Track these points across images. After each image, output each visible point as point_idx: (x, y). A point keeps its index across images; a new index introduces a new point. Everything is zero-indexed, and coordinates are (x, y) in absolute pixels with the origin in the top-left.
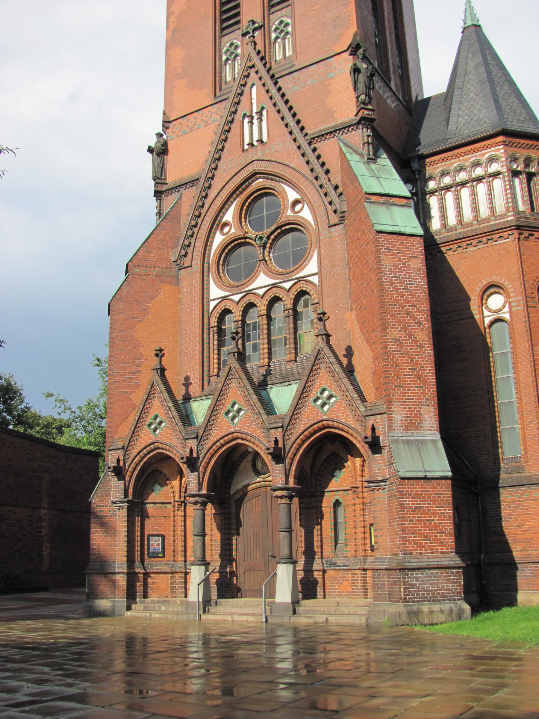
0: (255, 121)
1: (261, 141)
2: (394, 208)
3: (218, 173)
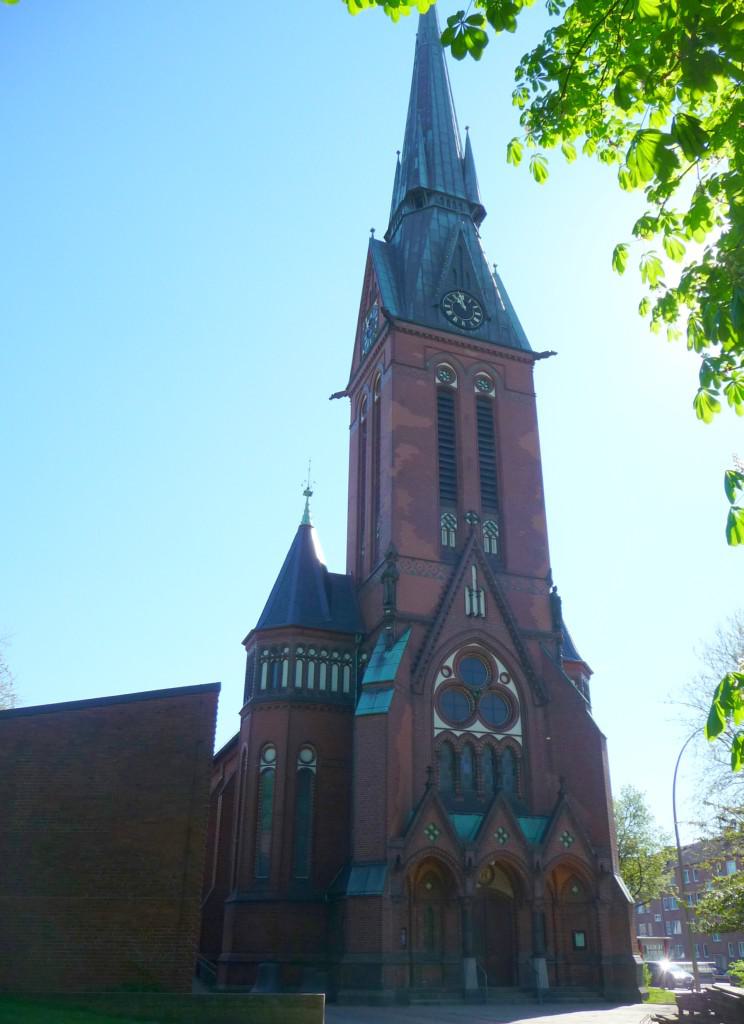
0: (475, 594)
1: (479, 614)
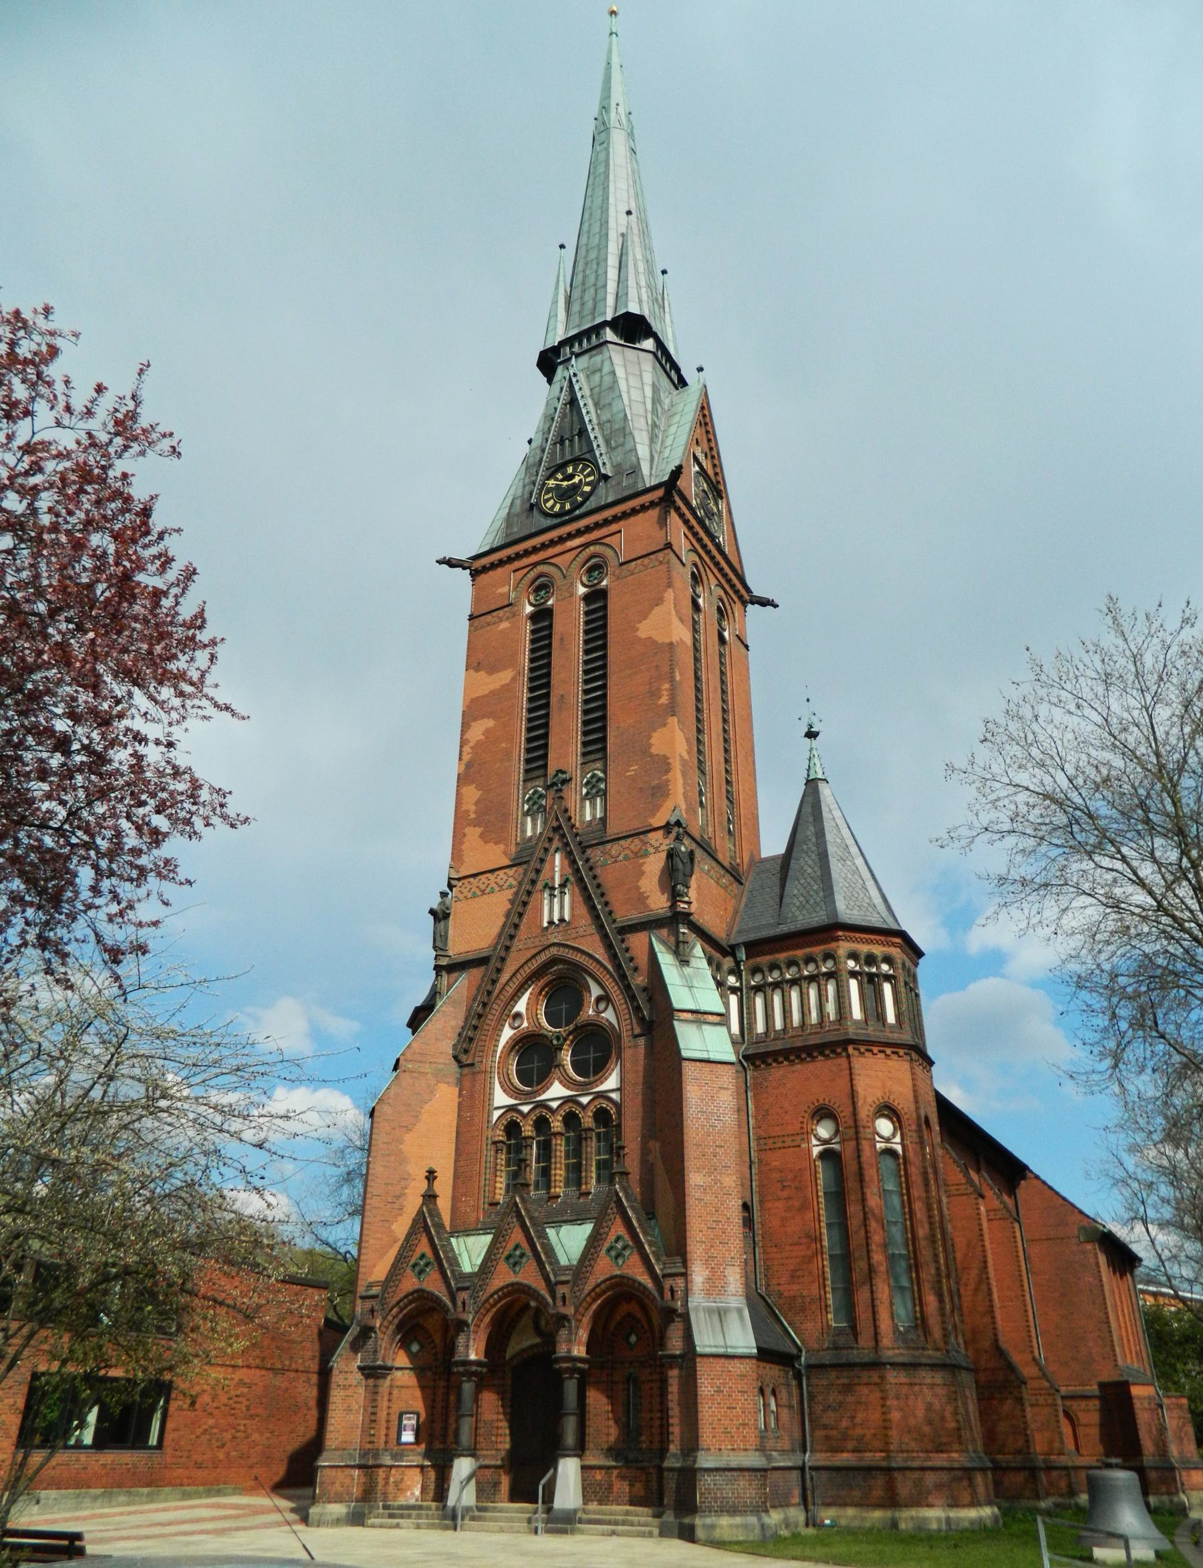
1: (562, 920)
2: (705, 1027)
3: (517, 944)
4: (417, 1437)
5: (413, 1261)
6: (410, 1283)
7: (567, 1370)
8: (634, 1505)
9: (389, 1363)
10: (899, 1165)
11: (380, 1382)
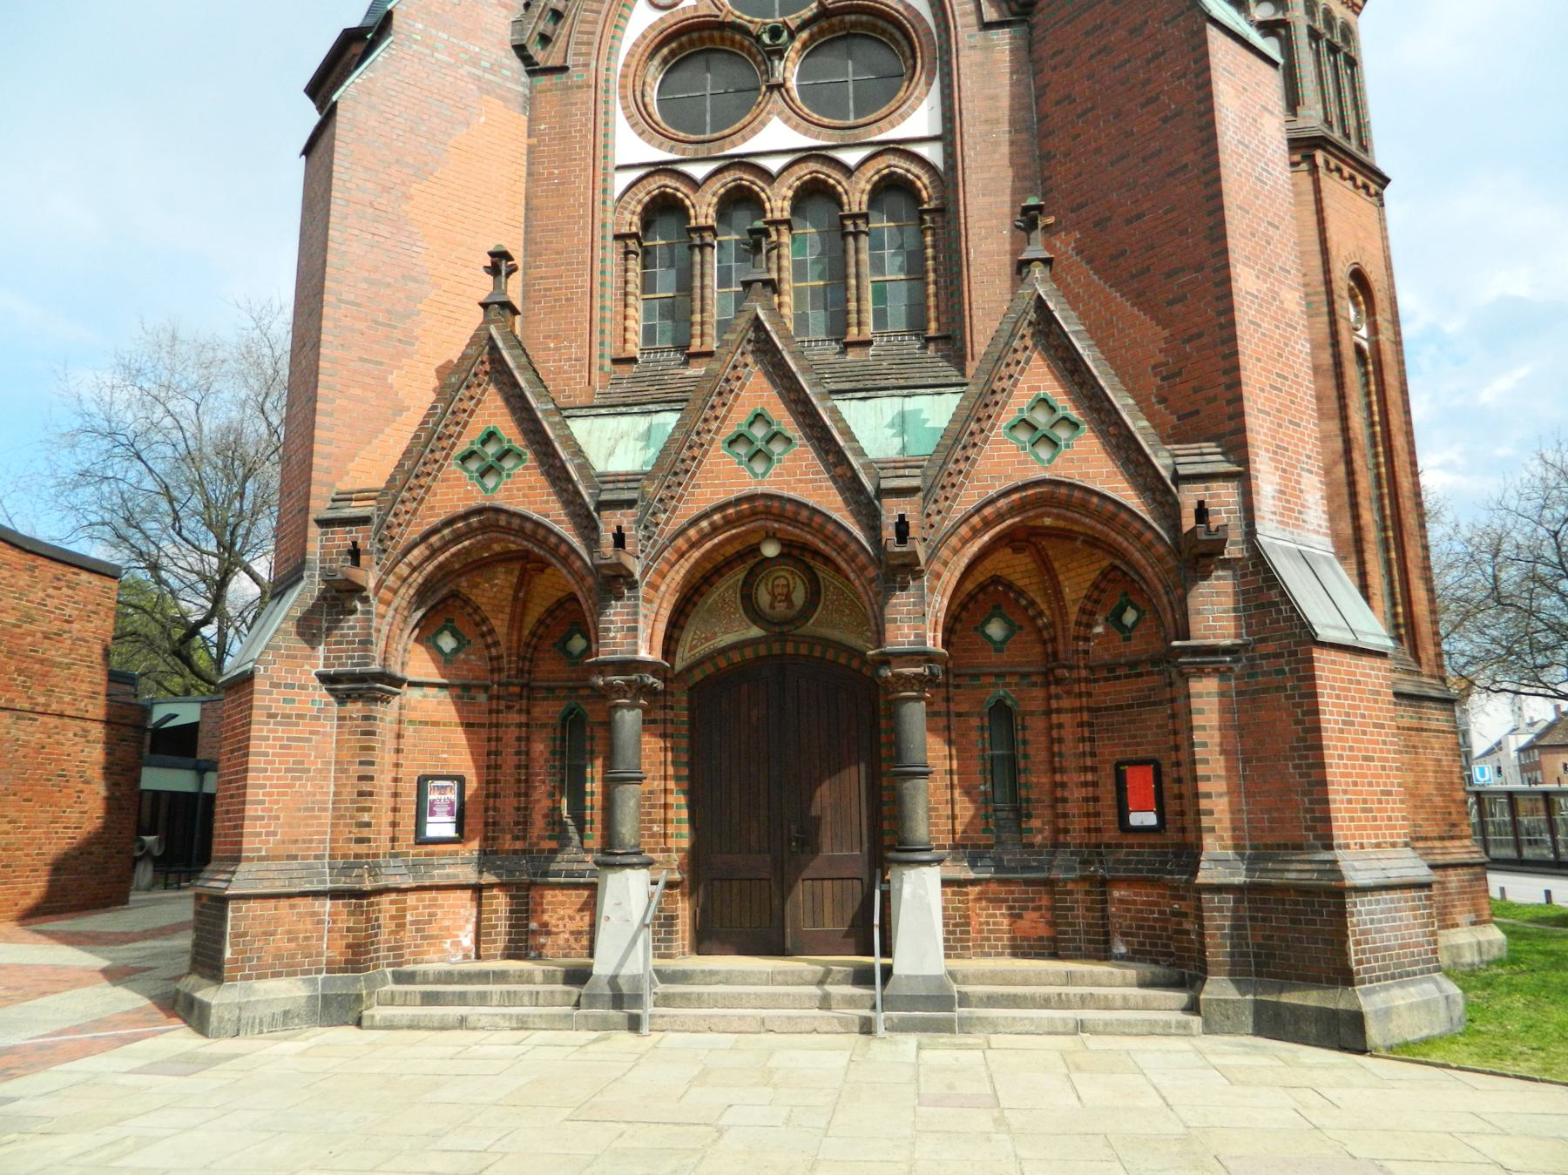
4: (460, 826)
5: (462, 446)
6: (456, 491)
7: (908, 681)
8: (1025, 956)
9: (396, 670)
10: (1366, 374)
11: (378, 709)
